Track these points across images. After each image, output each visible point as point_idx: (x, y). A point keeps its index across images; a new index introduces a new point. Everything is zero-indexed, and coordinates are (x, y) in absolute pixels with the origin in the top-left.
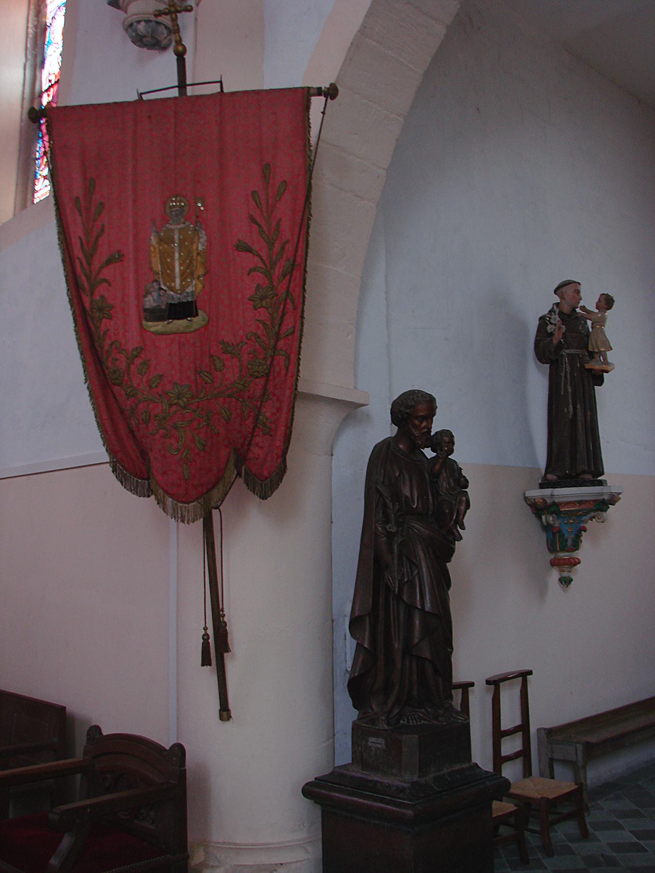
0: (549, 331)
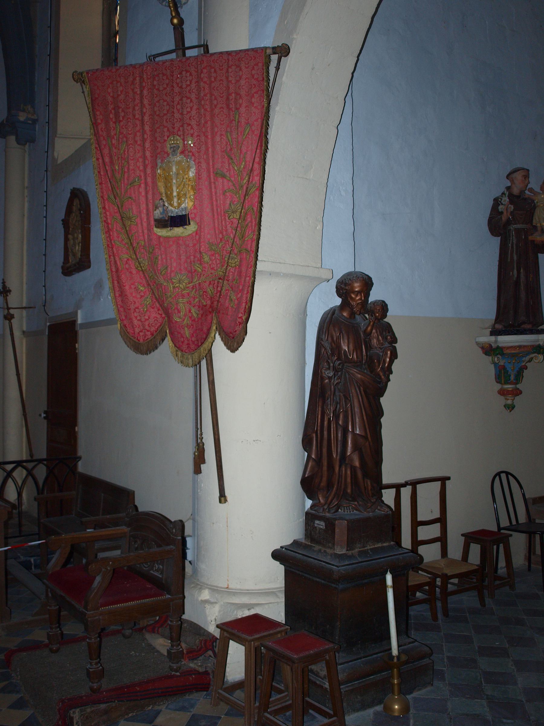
0: (500, 210)
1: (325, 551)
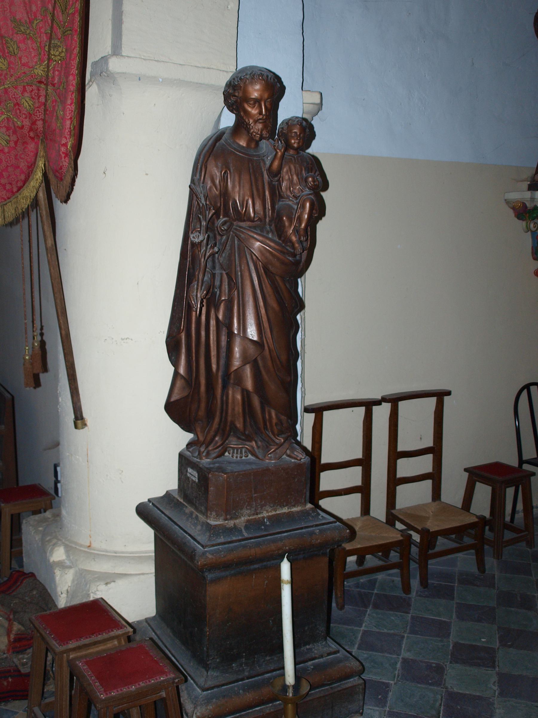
1: (197, 517)
